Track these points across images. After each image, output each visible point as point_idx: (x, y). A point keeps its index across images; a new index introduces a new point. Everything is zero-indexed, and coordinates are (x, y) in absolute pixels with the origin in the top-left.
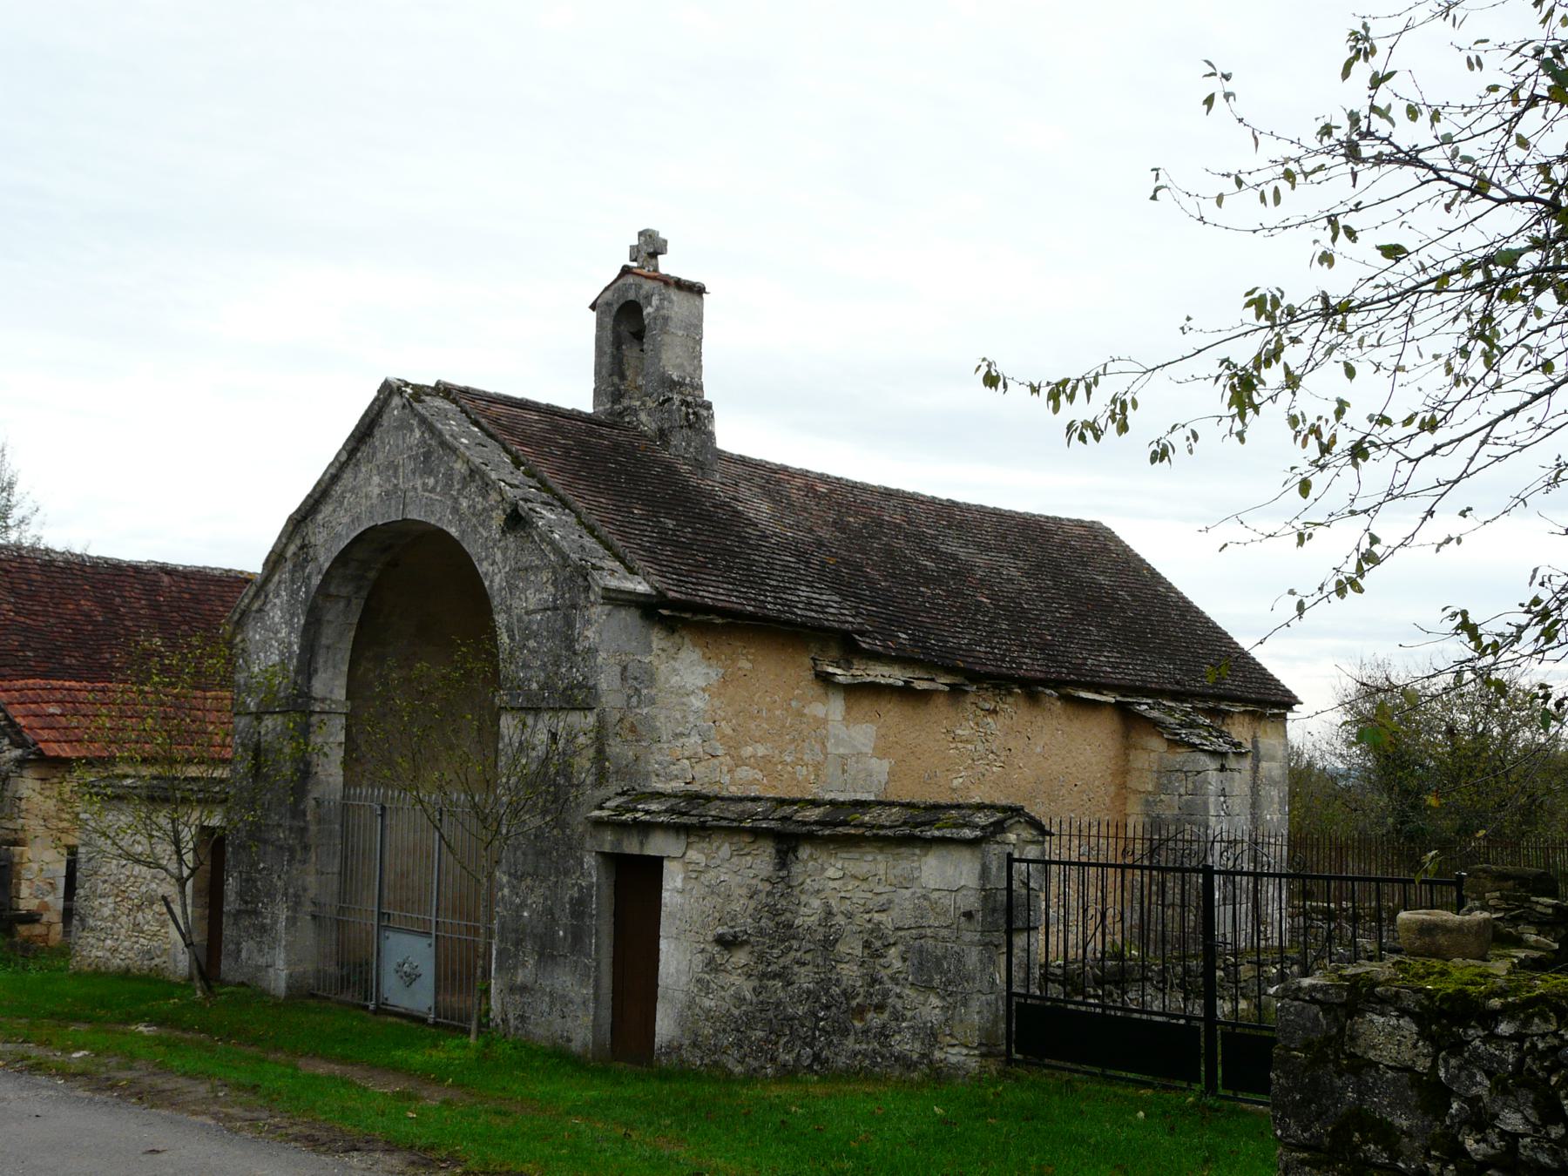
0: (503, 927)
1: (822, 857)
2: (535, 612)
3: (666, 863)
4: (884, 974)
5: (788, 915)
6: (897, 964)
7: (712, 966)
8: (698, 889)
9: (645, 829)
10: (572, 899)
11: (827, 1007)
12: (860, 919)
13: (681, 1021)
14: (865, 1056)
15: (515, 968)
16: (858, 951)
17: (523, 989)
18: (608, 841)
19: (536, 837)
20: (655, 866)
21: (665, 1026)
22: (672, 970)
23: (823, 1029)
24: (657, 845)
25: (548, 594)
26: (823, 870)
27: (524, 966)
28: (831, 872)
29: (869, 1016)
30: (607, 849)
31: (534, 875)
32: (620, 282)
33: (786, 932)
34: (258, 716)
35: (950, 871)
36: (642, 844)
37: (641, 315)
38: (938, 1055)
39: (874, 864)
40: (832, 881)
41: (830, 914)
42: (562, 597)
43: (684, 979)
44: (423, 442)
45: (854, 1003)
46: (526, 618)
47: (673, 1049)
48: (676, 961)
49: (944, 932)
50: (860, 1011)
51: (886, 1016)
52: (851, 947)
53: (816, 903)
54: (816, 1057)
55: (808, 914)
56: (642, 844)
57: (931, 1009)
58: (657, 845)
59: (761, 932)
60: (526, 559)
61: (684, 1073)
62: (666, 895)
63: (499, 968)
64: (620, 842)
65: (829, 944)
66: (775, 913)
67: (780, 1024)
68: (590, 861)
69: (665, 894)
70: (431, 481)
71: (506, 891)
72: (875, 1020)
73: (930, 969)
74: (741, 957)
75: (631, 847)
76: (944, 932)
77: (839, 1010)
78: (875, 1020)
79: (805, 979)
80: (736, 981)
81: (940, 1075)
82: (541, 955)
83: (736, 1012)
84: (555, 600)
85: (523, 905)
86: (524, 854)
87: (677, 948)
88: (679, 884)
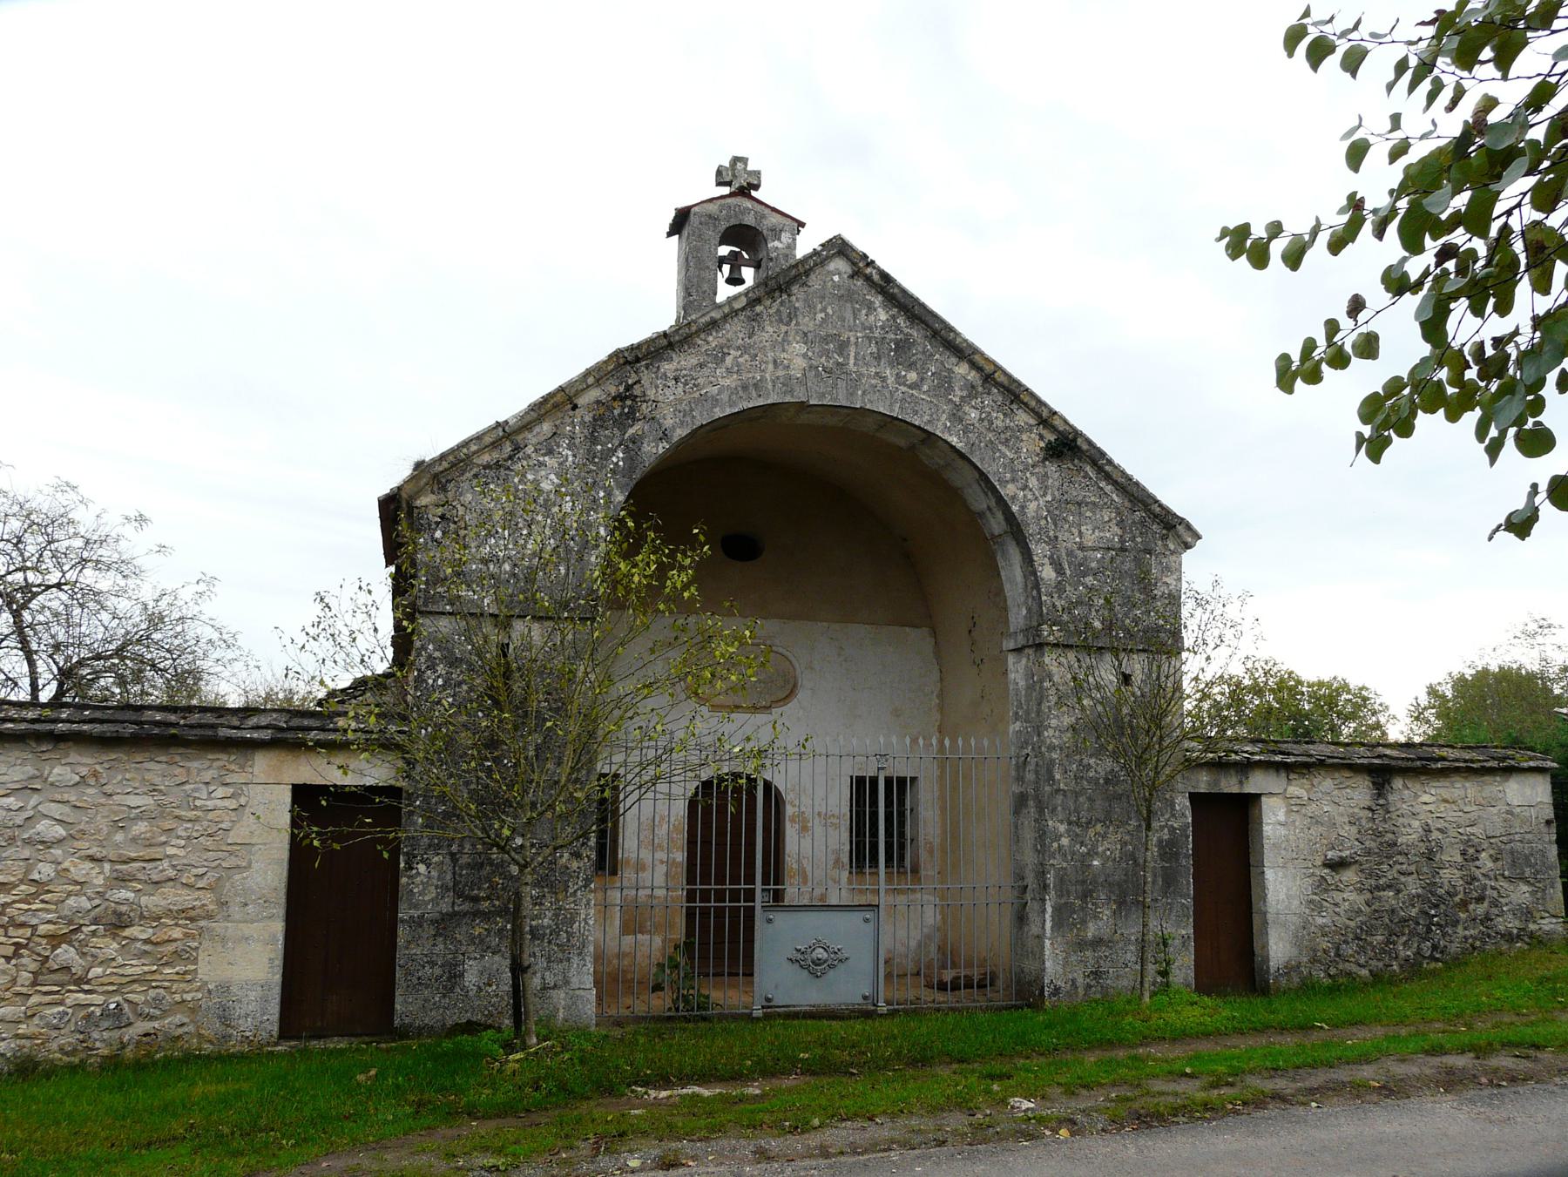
0: (1061, 880)
1: (1414, 785)
2: (1094, 549)
3: (1264, 799)
4: (1478, 873)
5: (1390, 836)
6: (1490, 865)
7: (1322, 885)
8: (1295, 826)
9: (1246, 767)
10: (1160, 841)
11: (1436, 906)
12: (1452, 833)
13: (1297, 941)
14: (1475, 938)
15: (1084, 922)
16: (1459, 859)
17: (1098, 942)
18: (1203, 782)
19: (1107, 781)
20: (1246, 806)
21: (1278, 948)
22: (1282, 896)
23: (1438, 924)
24: (1256, 783)
25: (1113, 534)
26: (1416, 796)
27: (1096, 917)
28: (1426, 798)
29: (1471, 907)
30: (1203, 788)
31: (1107, 819)
32: (729, 200)
33: (1391, 849)
34: (503, 622)
35: (1528, 792)
36: (1241, 783)
37: (670, 234)
38: (1532, 927)
39: (1464, 790)
40: (1423, 805)
41: (1427, 830)
42: (1133, 539)
43: (1296, 902)
44: (892, 323)
45: (1457, 899)
46: (1080, 554)
47: (1290, 968)
48: (1283, 888)
49: (1529, 836)
50: (1464, 905)
51: (1486, 904)
52: (1452, 855)
53: (1416, 824)
54: (1435, 947)
55: (1410, 835)
56: (1241, 783)
57: (1521, 894)
58: (1256, 783)
59: (1369, 852)
60: (1075, 493)
61: (1307, 988)
62: (1267, 829)
63: (1058, 924)
64: (1217, 782)
65: (1429, 856)
66: (1378, 834)
67: (1398, 926)
68: (1182, 803)
69: (1265, 828)
70: (912, 376)
71: (1065, 841)
72: (1481, 909)
73: (1518, 865)
74: (1350, 876)
75: (1230, 785)
76: (1529, 836)
77: (1438, 907)
78: (1481, 909)
79: (1413, 886)
80: (1350, 895)
81: (1538, 941)
82: (1121, 903)
83: (1352, 924)
84: (1122, 541)
85: (1093, 853)
86: (1090, 799)
87: (1285, 876)
88: (1281, 817)
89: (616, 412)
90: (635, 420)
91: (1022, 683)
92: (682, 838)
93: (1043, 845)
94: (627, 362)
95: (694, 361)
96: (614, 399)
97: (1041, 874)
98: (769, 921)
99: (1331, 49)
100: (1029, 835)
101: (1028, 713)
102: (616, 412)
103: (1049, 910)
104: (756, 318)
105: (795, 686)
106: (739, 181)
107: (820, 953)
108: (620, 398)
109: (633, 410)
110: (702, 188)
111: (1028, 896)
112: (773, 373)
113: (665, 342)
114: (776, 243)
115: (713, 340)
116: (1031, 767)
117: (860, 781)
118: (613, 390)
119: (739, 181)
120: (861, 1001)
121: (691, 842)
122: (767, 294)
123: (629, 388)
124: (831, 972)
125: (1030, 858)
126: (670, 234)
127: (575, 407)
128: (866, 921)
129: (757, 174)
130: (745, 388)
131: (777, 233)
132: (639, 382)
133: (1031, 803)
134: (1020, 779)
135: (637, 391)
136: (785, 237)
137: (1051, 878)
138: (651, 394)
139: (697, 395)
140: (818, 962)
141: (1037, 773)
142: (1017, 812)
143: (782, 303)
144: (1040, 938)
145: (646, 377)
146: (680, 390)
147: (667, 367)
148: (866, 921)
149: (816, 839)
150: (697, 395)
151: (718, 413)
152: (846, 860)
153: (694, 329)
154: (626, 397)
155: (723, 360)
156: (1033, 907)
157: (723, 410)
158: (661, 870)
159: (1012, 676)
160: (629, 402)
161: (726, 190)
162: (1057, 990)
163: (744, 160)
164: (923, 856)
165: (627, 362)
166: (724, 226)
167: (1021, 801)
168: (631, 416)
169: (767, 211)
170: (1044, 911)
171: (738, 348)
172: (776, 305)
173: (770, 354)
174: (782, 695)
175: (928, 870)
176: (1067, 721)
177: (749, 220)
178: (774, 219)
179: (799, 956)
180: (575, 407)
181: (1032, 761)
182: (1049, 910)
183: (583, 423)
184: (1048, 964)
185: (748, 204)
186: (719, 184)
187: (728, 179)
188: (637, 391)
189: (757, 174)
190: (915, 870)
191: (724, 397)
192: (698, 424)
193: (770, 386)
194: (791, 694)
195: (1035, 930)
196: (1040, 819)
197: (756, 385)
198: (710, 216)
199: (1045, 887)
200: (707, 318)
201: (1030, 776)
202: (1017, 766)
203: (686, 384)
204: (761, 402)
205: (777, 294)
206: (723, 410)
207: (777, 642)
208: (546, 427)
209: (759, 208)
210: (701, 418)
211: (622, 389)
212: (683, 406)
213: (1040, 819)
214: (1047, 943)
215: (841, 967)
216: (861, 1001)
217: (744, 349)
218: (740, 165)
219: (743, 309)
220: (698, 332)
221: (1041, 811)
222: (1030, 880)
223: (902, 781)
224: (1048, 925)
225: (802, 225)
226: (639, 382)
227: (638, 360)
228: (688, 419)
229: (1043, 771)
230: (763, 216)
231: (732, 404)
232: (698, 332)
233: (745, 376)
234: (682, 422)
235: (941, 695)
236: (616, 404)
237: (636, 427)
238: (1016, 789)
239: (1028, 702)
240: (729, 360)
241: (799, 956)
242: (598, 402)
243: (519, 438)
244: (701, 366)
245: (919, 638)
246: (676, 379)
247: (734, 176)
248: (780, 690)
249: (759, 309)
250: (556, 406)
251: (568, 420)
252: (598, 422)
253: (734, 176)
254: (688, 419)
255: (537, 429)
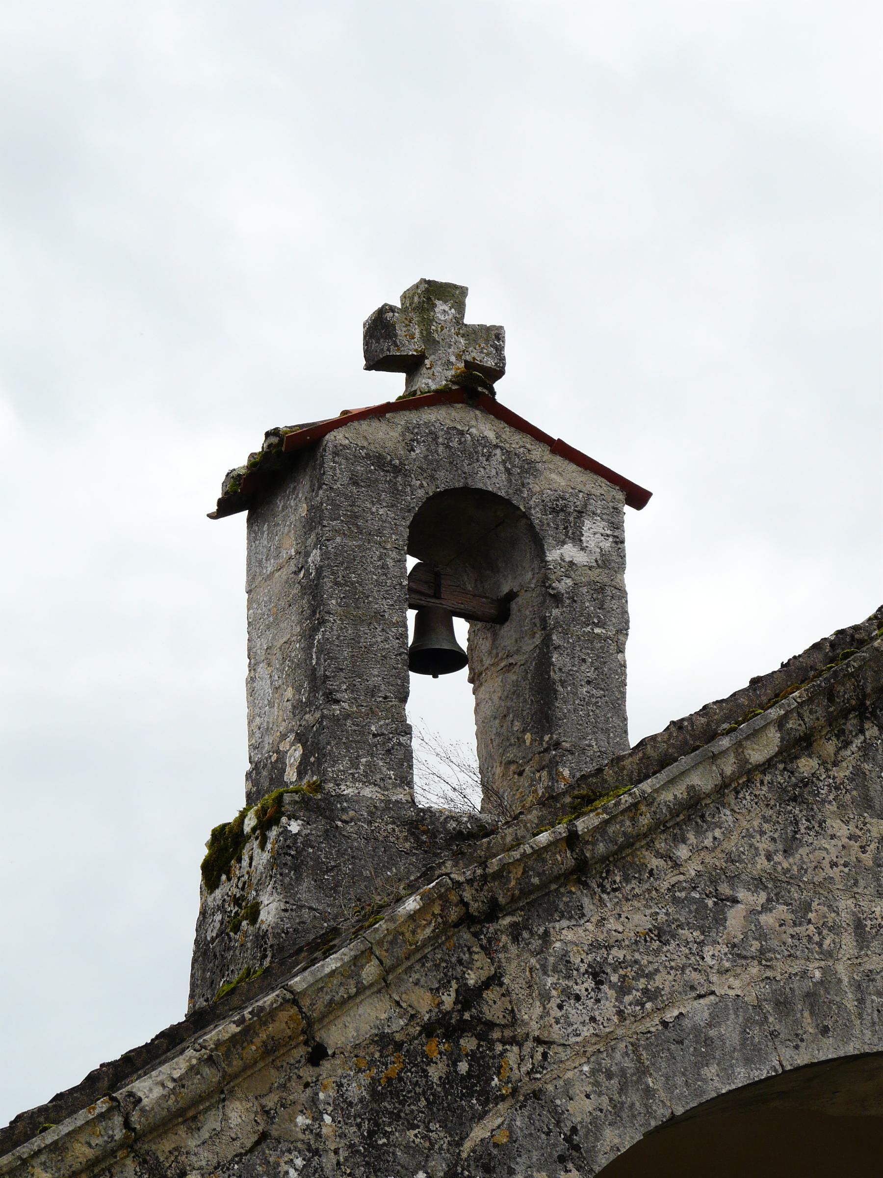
32: (430, 415)
37: (225, 508)
89: (436, 1072)
90: (489, 1098)
94: (468, 920)
95: (641, 920)
96: (428, 1030)
102: (436, 1072)
104: (799, 793)
106: (432, 345)
108: (442, 1027)
109: (484, 1065)
110: (334, 381)
112: (855, 963)
113: (566, 859)
114: (569, 551)
115: (691, 856)
118: (423, 1003)
119: (432, 345)
122: (831, 720)
123: (469, 997)
126: (225, 508)
127: (318, 1055)
129: (494, 337)
130: (783, 1005)
131: (569, 518)
132: (494, 980)
135: (493, 1007)
136: (593, 531)
138: (531, 1015)
139: (652, 1024)
143: (866, 750)
145: (516, 965)
146: (608, 1007)
147: (571, 936)
150: (652, 1024)
151: (717, 1082)
153: (645, 821)
154: (463, 1028)
155: (720, 920)
157: (727, 1074)
160: (468, 1043)
161: (391, 386)
163: (454, 295)
165: (468, 920)
166: (419, 491)
168: (476, 1087)
169: (539, 452)
171: (758, 884)
172: (851, 756)
173: (845, 904)
177: (491, 477)
178: (559, 478)
180: (318, 1055)
183: (342, 1105)
185: (485, 428)
186: (377, 361)
187: (411, 348)
188: (493, 1007)
189: (494, 337)
191: (729, 1031)
192: (662, 1113)
193: (850, 1002)
197: (810, 997)
198: (379, 460)
200: (679, 791)
203: (623, 990)
204: (828, 1050)
205: (851, 724)
206: (727, 1074)
208: (238, 1115)
209: (516, 441)
210: (672, 1100)
211: (448, 1000)
212: (621, 1060)
217: (775, 886)
218: (442, 310)
219: (767, 766)
220: (660, 826)
225: (639, 497)
226: (494, 980)
227: (493, 911)
228: (634, 1097)
230: (530, 468)
231: (752, 1054)
232: (647, 837)
233: (781, 968)
234: (617, 1107)
236: (435, 1047)
237: (492, 1122)
240: (735, 918)
242: (383, 1040)
243: (164, 1147)
244: (662, 933)
246: (597, 974)
247: (429, 339)
249: (806, 765)
250: (270, 1050)
251: (302, 1096)
252: (386, 1102)
253: (429, 339)
254: (634, 1097)
255: (212, 1122)
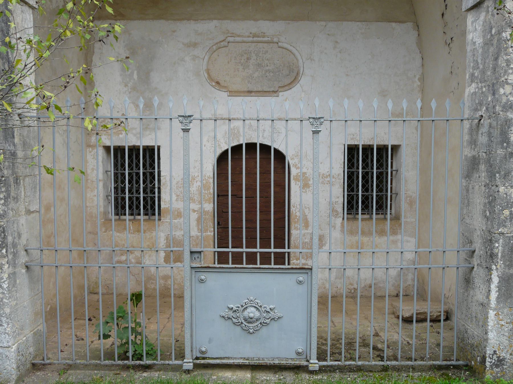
91: (479, 41)
92: (212, 189)
93: (492, 212)
97: (489, 242)
98: (202, 281)
99: (444, 320)
100: (478, 200)
101: (483, 72)
103: (495, 280)
105: (298, 74)
107: (251, 312)
111: (475, 261)
116: (484, 129)
117: (352, 150)
120: (294, 356)
121: (221, 195)
124: (264, 330)
125: (478, 223)
128: (300, 283)
133: (482, 167)
134: (473, 143)
137: (499, 247)
140: (249, 320)
141: (490, 135)
142: (468, 176)
144: (484, 306)
148: (300, 283)
149: (315, 191)
152: (340, 210)
156: (479, 273)
158: (194, 216)
159: (470, 37)
162: (500, 362)
164: (404, 206)
167: (473, 164)
170: (489, 281)
174: (287, 81)
175: (409, 218)
176: (487, 376)
179: (231, 314)
181: (485, 122)
182: (495, 280)
184: (491, 335)
190: (397, 218)
194: (295, 80)
195: (480, 297)
196: (491, 184)
199: (492, 256)
201: (483, 139)
202: (471, 129)
207: (282, 39)
213: (491, 184)
214: (492, 314)
215: (274, 325)
216: (294, 356)
221: (492, 176)
222: (478, 245)
223: (382, 149)
224: (494, 295)
229: (496, 133)
235: (422, 79)
238: (468, 152)
239: (484, 59)
241: (231, 314)
245: (404, 32)
248: (285, 78)
